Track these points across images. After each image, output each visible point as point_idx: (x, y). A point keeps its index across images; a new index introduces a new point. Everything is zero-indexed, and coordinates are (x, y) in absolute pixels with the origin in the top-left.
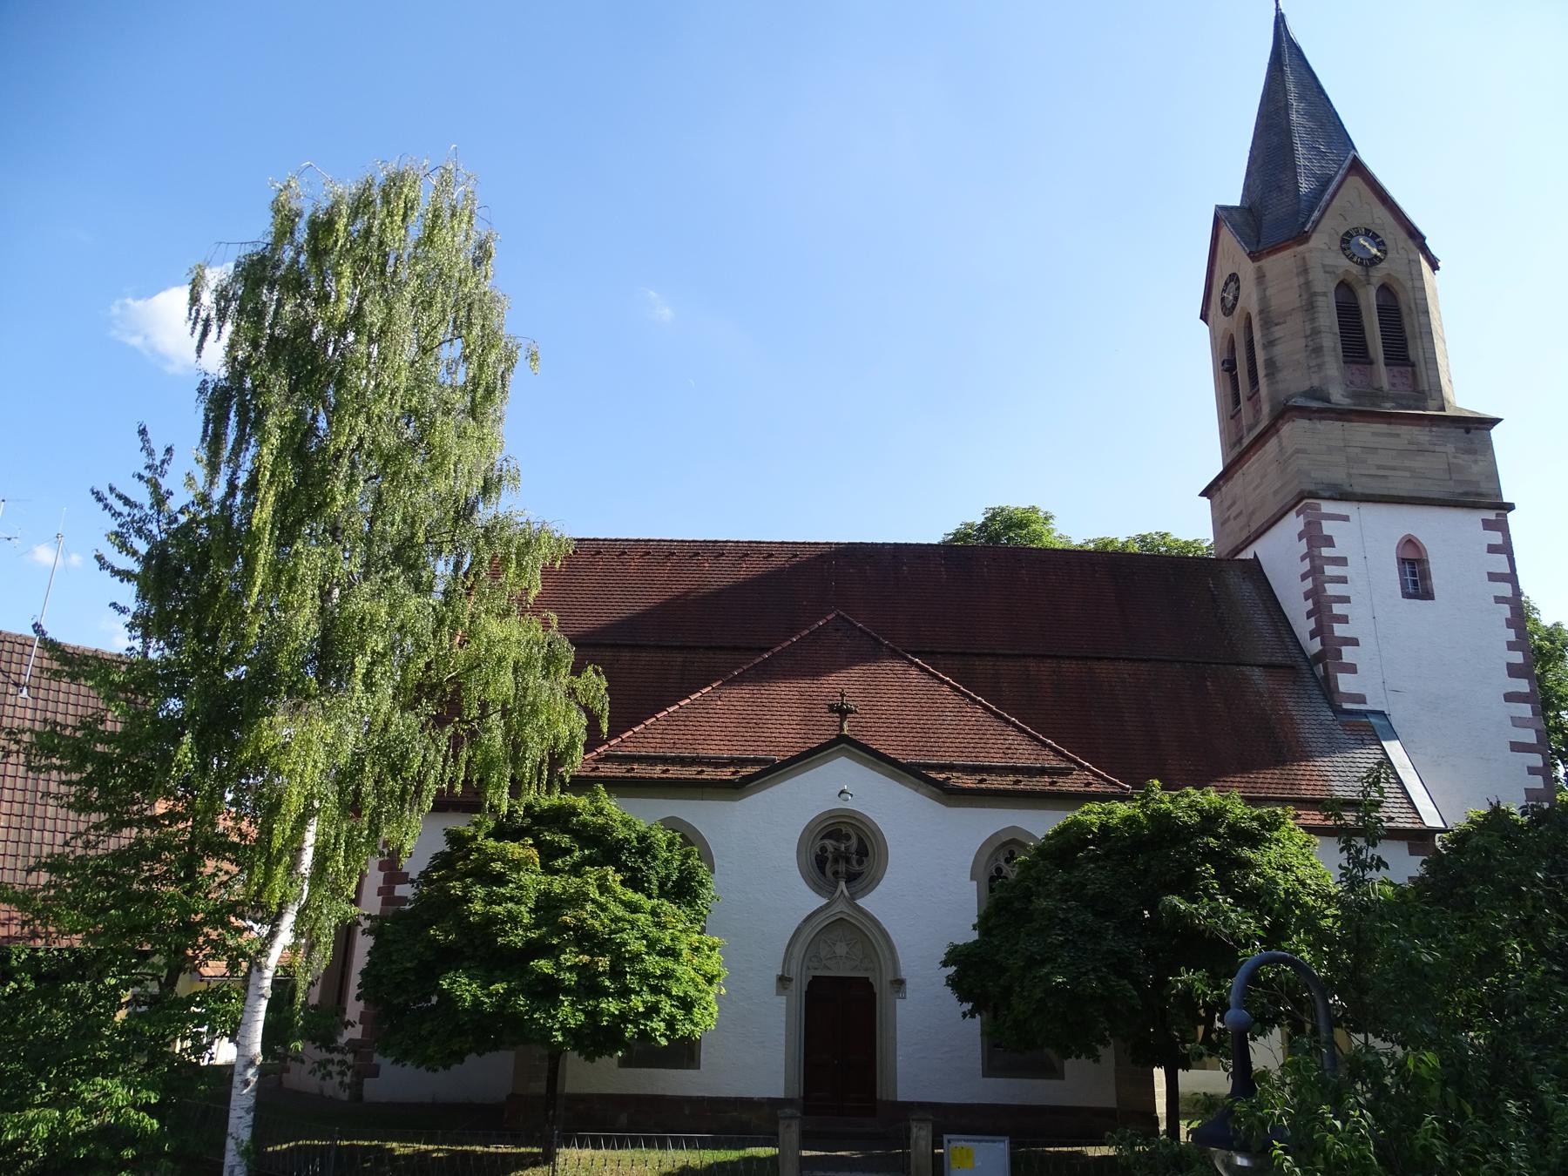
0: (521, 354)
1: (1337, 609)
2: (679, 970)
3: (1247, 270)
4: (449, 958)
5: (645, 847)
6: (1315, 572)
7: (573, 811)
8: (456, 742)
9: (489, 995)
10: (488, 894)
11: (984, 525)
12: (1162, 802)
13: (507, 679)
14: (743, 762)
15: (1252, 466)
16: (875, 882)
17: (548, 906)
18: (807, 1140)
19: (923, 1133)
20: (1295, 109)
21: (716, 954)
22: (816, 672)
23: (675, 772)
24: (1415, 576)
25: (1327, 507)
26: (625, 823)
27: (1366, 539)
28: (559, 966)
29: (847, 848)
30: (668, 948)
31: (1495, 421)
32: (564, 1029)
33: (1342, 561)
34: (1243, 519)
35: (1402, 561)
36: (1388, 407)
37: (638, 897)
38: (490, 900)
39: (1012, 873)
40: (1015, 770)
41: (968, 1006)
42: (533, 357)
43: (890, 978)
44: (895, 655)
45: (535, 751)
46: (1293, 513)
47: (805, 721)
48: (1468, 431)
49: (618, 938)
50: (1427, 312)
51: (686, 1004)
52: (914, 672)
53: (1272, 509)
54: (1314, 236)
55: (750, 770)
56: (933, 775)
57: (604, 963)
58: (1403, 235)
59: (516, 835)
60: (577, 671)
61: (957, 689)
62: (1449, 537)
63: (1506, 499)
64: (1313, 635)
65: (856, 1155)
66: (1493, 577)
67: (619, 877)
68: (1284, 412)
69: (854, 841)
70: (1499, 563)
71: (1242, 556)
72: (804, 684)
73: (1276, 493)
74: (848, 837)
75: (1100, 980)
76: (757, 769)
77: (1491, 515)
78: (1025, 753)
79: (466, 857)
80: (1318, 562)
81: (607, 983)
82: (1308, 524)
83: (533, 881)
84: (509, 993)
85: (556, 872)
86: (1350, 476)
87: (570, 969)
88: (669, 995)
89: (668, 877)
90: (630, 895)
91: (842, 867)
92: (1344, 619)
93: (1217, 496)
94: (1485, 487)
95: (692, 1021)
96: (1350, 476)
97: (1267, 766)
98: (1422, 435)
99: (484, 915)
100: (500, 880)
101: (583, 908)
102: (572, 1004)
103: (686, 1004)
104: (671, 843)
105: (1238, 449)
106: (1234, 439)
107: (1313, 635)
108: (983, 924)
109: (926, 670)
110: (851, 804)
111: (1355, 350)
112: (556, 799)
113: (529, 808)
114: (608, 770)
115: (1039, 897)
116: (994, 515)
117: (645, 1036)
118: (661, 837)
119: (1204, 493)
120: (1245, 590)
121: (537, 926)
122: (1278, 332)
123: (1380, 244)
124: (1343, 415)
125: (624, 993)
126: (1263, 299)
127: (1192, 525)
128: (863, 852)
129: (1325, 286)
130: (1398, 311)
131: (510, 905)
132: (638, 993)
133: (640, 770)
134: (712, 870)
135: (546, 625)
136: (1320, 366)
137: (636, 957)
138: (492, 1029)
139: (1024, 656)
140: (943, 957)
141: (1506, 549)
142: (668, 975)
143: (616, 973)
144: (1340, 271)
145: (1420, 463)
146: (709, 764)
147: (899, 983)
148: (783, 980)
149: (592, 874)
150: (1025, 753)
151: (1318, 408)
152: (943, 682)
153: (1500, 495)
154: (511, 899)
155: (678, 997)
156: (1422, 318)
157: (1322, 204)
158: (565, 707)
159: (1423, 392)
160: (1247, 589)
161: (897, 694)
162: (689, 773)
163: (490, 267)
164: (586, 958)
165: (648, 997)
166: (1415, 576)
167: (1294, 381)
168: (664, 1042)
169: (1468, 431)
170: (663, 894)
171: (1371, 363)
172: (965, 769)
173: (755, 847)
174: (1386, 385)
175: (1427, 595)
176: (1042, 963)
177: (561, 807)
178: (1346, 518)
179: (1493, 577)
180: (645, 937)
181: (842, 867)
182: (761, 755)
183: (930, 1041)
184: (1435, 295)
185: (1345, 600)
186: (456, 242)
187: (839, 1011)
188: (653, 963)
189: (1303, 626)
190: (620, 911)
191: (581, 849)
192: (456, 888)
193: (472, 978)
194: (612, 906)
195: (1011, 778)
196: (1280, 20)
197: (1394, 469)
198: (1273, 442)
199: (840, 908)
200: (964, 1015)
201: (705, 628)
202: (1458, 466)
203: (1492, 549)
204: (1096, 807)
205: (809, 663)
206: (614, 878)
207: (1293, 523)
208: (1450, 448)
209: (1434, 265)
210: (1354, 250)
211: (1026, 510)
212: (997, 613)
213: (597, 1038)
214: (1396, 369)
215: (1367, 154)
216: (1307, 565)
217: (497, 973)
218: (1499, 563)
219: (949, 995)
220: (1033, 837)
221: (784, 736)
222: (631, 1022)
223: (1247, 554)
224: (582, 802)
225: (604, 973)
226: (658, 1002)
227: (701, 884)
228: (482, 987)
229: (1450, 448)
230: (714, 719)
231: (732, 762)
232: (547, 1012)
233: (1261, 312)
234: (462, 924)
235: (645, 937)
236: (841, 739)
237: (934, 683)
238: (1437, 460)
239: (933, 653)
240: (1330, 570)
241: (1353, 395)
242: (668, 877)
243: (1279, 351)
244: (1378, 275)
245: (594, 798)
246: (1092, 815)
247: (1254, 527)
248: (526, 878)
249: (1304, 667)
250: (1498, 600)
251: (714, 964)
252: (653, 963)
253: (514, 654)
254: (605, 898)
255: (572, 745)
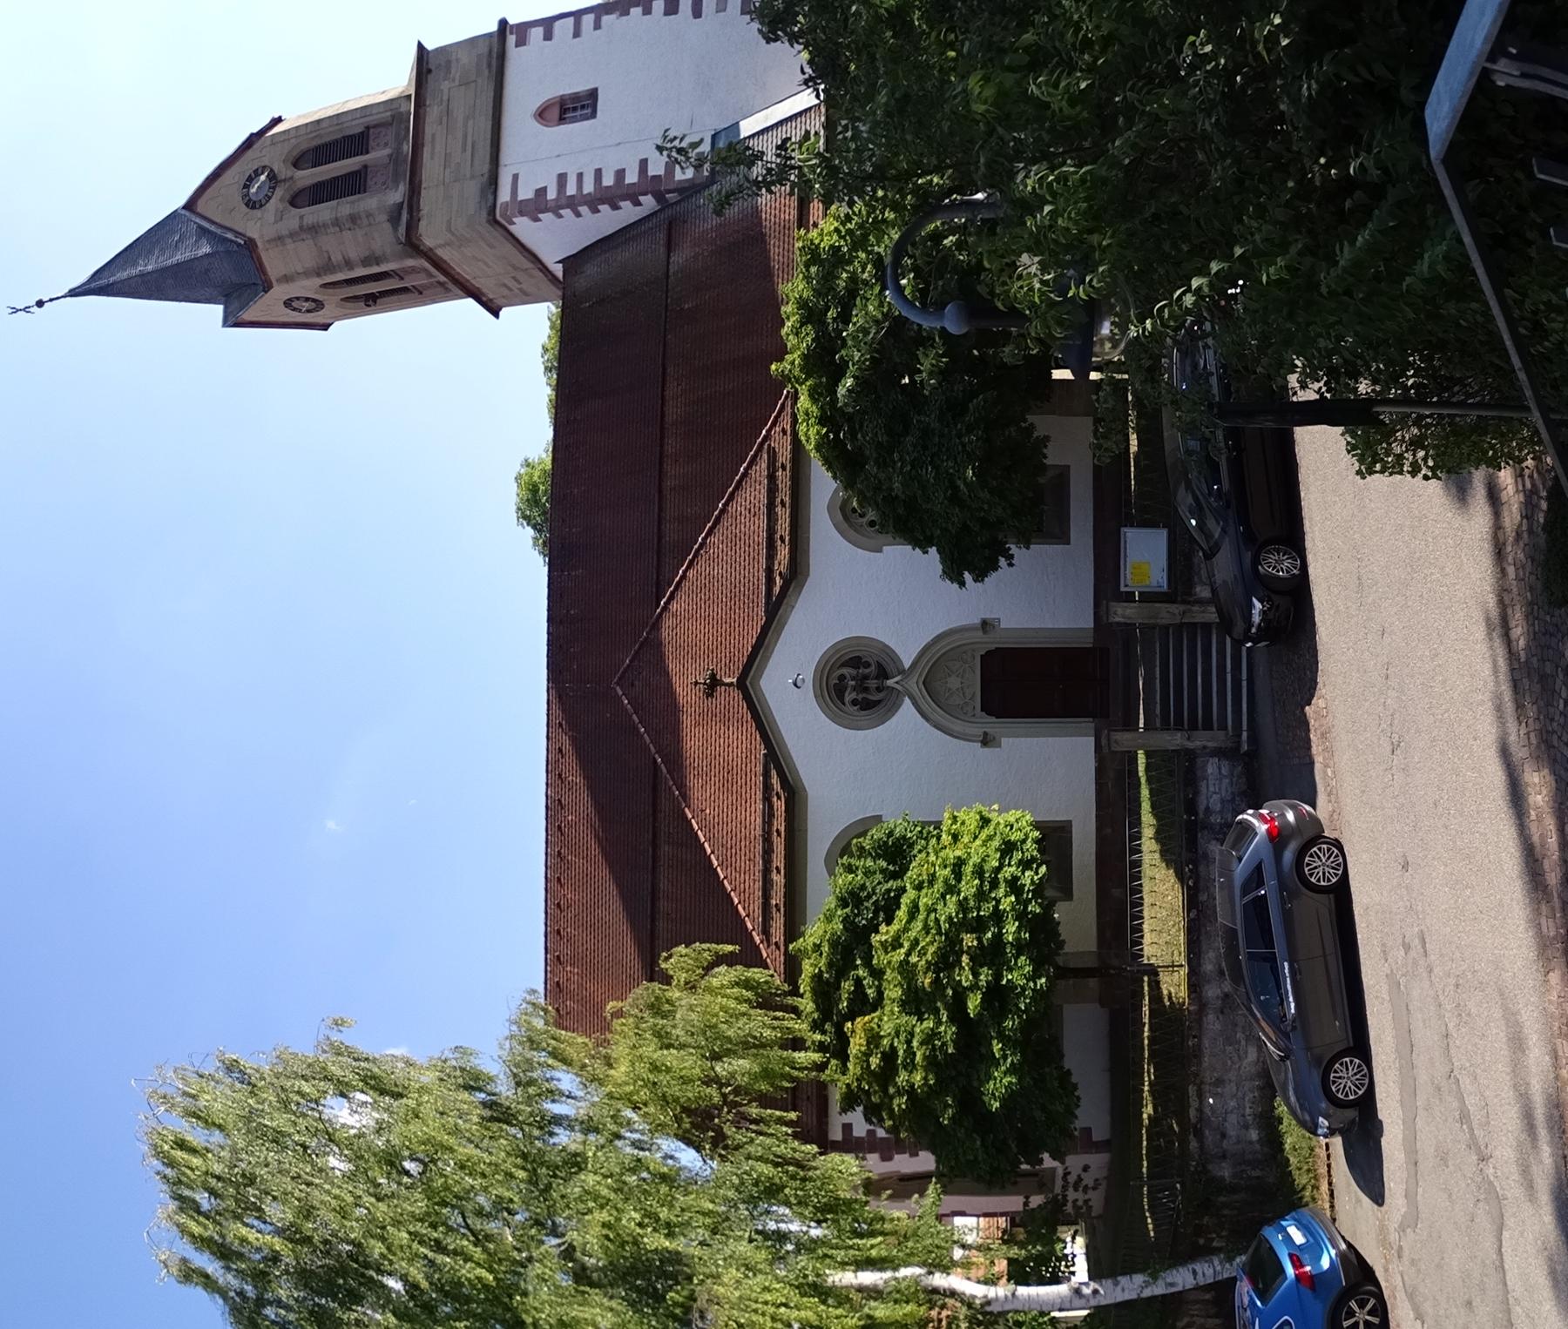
0: (335, 1037)
1: (608, 181)
2: (975, 859)
3: (280, 292)
4: (970, 1102)
5: (852, 899)
6: (573, 204)
7: (817, 978)
8: (742, 1120)
9: (1005, 1057)
10: (905, 1068)
11: (534, 527)
12: (793, 363)
13: (670, 1057)
14: (767, 787)
15: (465, 270)
16: (886, 649)
17: (915, 1002)
18: (1130, 724)
19: (1120, 611)
20: (145, 271)
21: (961, 815)
22: (672, 709)
23: (778, 860)
24: (576, 107)
25: (504, 195)
26: (829, 919)
27: (536, 157)
28: (974, 987)
29: (853, 679)
30: (953, 871)
31: (420, 46)
32: (1033, 977)
33: (562, 179)
34: (520, 276)
35: (562, 120)
36: (408, 148)
37: (905, 900)
38: (910, 1066)
39: (872, 515)
40: (771, 506)
41: (1002, 561)
42: (338, 1023)
43: (980, 633)
44: (656, 626)
45: (760, 1024)
46: (512, 228)
47: (725, 721)
48: (430, 71)
49: (945, 926)
50: (318, 122)
51: (1008, 848)
52: (674, 606)
53: (509, 248)
54: (249, 234)
55: (775, 780)
56: (777, 589)
57: (969, 940)
58: (250, 154)
59: (843, 1040)
60: (666, 979)
61: (691, 562)
62: (532, 79)
63: (494, 27)
64: (637, 203)
65: (1141, 672)
66: (577, 33)
67: (883, 928)
68: (412, 245)
69: (845, 671)
70: (563, 28)
71: (560, 275)
72: (687, 721)
73: (492, 247)
74: (842, 678)
75: (970, 430)
76: (774, 773)
77: (511, 39)
78: (754, 494)
79: (867, 1093)
80: (563, 201)
81: (989, 935)
82: (522, 214)
83: (890, 1020)
84: (1002, 1037)
85: (880, 993)
86: (472, 177)
87: (976, 974)
88: (998, 869)
89: (883, 871)
90: (902, 913)
91: (872, 684)
92: (620, 174)
93: (499, 302)
94: (483, 49)
95: (1024, 841)
96: (472, 177)
97: (765, 253)
98: (433, 113)
99: (926, 1069)
100: (889, 1057)
101: (915, 965)
102: (1010, 970)
103: (1008, 848)
104: (850, 869)
105: (450, 285)
106: (440, 289)
107: (637, 203)
108: (922, 544)
109: (672, 593)
110: (808, 675)
111: (353, 184)
112: (807, 1004)
113: (816, 1026)
114: (778, 933)
115: (892, 489)
116: (525, 517)
117: (1038, 890)
118: (844, 880)
119: (496, 314)
120: (592, 271)
121: (936, 1012)
122: (337, 258)
123: (257, 173)
124: (414, 191)
125: (998, 917)
126: (307, 274)
127: (532, 325)
128: (856, 662)
129: (294, 218)
130: (317, 149)
131: (915, 1044)
132: (998, 902)
133: (777, 898)
134: (878, 819)
135: (619, 1014)
136: (369, 215)
137: (963, 906)
138: (1040, 1048)
139: (660, 492)
140: (956, 586)
141: (548, 24)
142: (979, 872)
143: (978, 926)
144: (281, 207)
145: (459, 112)
146: (770, 824)
147: (985, 625)
148: (986, 741)
149: (880, 958)
150: (754, 494)
151: (408, 214)
152: (684, 577)
153: (490, 35)
154: (909, 1042)
155: (1002, 858)
156: (324, 125)
157: (219, 231)
158: (706, 994)
159: (393, 117)
160: (592, 270)
161: (696, 626)
162: (779, 845)
163: (247, 1063)
164: (965, 959)
165: (1001, 891)
166: (576, 107)
167: (383, 238)
168: (1043, 869)
169: (430, 71)
170: (898, 875)
171: (365, 167)
172: (771, 557)
173: (857, 774)
174: (387, 151)
175: (593, 94)
176: (955, 488)
177: (814, 991)
178: (516, 177)
179: (577, 33)
180: (943, 896)
181: (872, 684)
182: (760, 769)
183: (1038, 595)
184: (304, 116)
185: (598, 173)
186: (221, 1099)
187: (1014, 685)
188: (968, 888)
189: (628, 213)
190: (918, 925)
191: (856, 967)
192: (900, 1103)
193: (990, 1077)
194: (912, 934)
195: (779, 509)
196: (74, 293)
197: (465, 136)
198: (440, 252)
199: (913, 684)
200: (1011, 565)
201: (636, 831)
202: (464, 79)
203: (548, 36)
204: (802, 428)
205: (664, 714)
206: (885, 933)
207: (522, 227)
208: (445, 86)
209: (277, 121)
210: (261, 196)
211: (519, 485)
212: (617, 516)
213: (1042, 937)
214: (371, 143)
215: (182, 200)
216: (566, 212)
217: (983, 1051)
218: (563, 28)
219: (992, 578)
220: (836, 491)
221: (741, 743)
222: (1026, 908)
223: (558, 270)
224: (808, 968)
225: (979, 939)
226: (1005, 880)
227: (891, 834)
228: (998, 1065)
229: (445, 86)
230: (722, 816)
231: (767, 799)
232: (1018, 996)
233: (319, 275)
234: (934, 1092)
235: (943, 896)
236: (741, 684)
237: (686, 585)
238: (455, 96)
239: (658, 583)
240: (571, 190)
241: (396, 183)
242: (883, 871)
243: (353, 255)
244: (283, 171)
245: (802, 953)
246: (810, 433)
247: (527, 264)
248: (888, 1028)
249: (669, 212)
250: (597, 26)
251: (972, 820)
252: (968, 888)
253: (650, 1050)
254: (906, 943)
255: (747, 984)
